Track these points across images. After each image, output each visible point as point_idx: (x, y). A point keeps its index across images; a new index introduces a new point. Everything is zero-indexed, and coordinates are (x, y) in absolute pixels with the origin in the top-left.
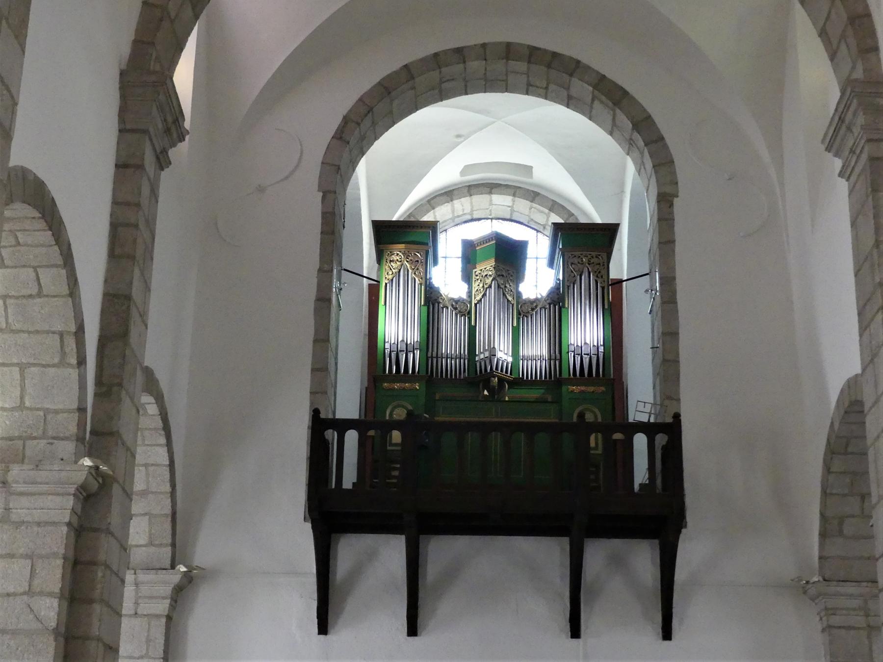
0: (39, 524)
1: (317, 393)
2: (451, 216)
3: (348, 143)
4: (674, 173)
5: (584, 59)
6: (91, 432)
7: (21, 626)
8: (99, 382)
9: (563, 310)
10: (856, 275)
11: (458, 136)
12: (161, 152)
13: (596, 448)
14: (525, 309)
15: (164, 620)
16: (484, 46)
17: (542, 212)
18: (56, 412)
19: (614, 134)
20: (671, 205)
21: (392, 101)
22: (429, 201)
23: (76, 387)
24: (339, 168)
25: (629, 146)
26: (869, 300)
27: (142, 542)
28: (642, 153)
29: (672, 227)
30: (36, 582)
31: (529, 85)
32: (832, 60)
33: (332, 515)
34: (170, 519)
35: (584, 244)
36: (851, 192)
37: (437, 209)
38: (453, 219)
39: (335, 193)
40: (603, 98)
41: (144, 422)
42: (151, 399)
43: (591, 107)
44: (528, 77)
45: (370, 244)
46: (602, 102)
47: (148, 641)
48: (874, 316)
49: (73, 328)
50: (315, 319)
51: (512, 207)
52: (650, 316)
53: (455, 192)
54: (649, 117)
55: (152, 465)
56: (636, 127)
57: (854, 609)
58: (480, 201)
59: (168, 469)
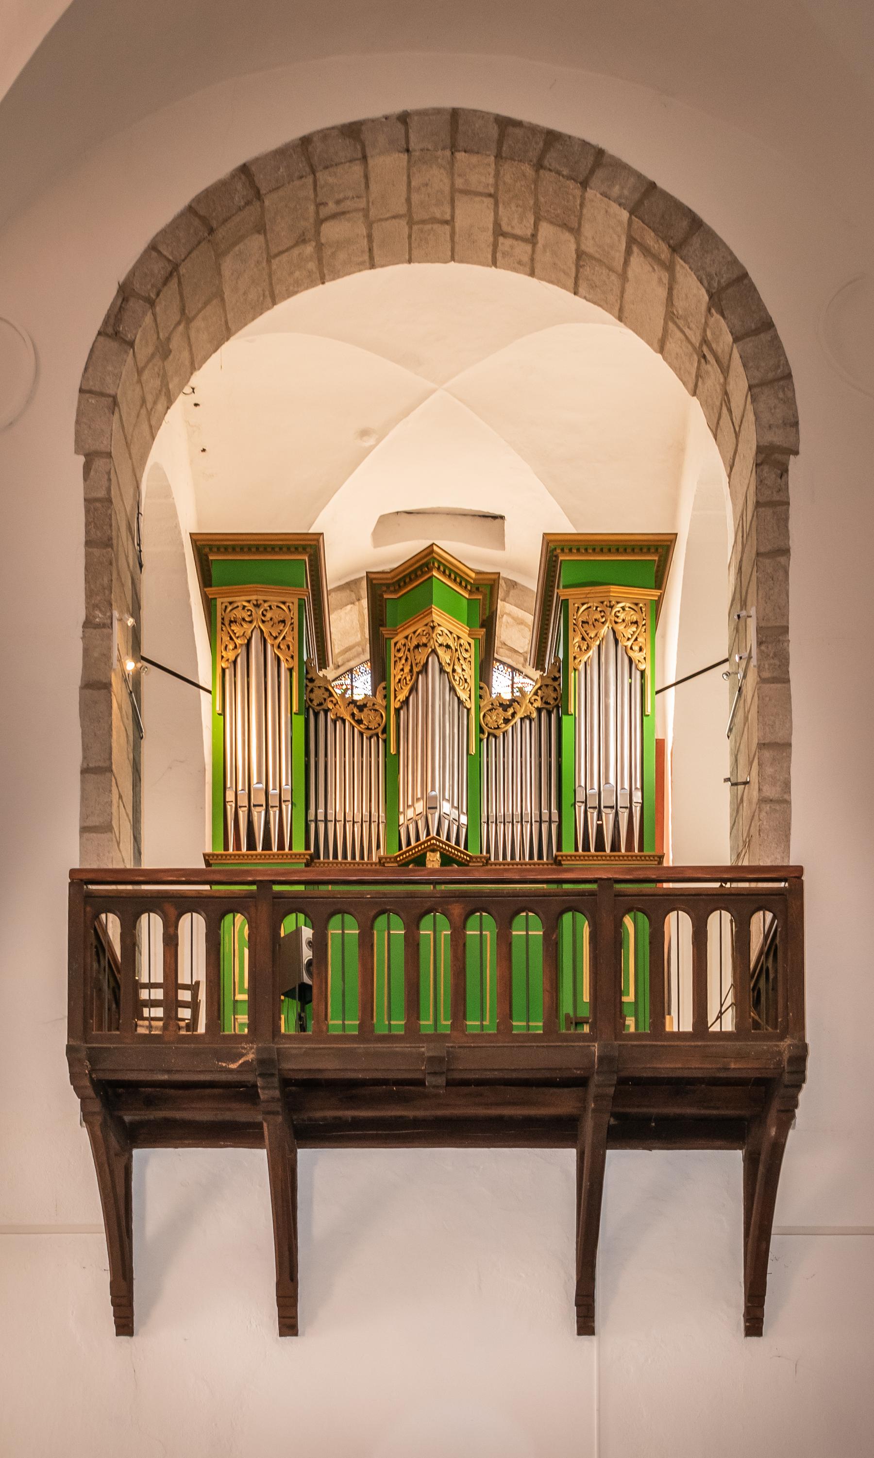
3: (131, 344)
4: (790, 402)
11: (364, 433)
16: (404, 118)
20: (783, 471)
21: (220, 255)
24: (115, 402)
28: (725, 371)
29: (783, 521)
31: (499, 232)
39: (109, 455)
43: (623, 277)
50: (82, 726)
52: (728, 741)
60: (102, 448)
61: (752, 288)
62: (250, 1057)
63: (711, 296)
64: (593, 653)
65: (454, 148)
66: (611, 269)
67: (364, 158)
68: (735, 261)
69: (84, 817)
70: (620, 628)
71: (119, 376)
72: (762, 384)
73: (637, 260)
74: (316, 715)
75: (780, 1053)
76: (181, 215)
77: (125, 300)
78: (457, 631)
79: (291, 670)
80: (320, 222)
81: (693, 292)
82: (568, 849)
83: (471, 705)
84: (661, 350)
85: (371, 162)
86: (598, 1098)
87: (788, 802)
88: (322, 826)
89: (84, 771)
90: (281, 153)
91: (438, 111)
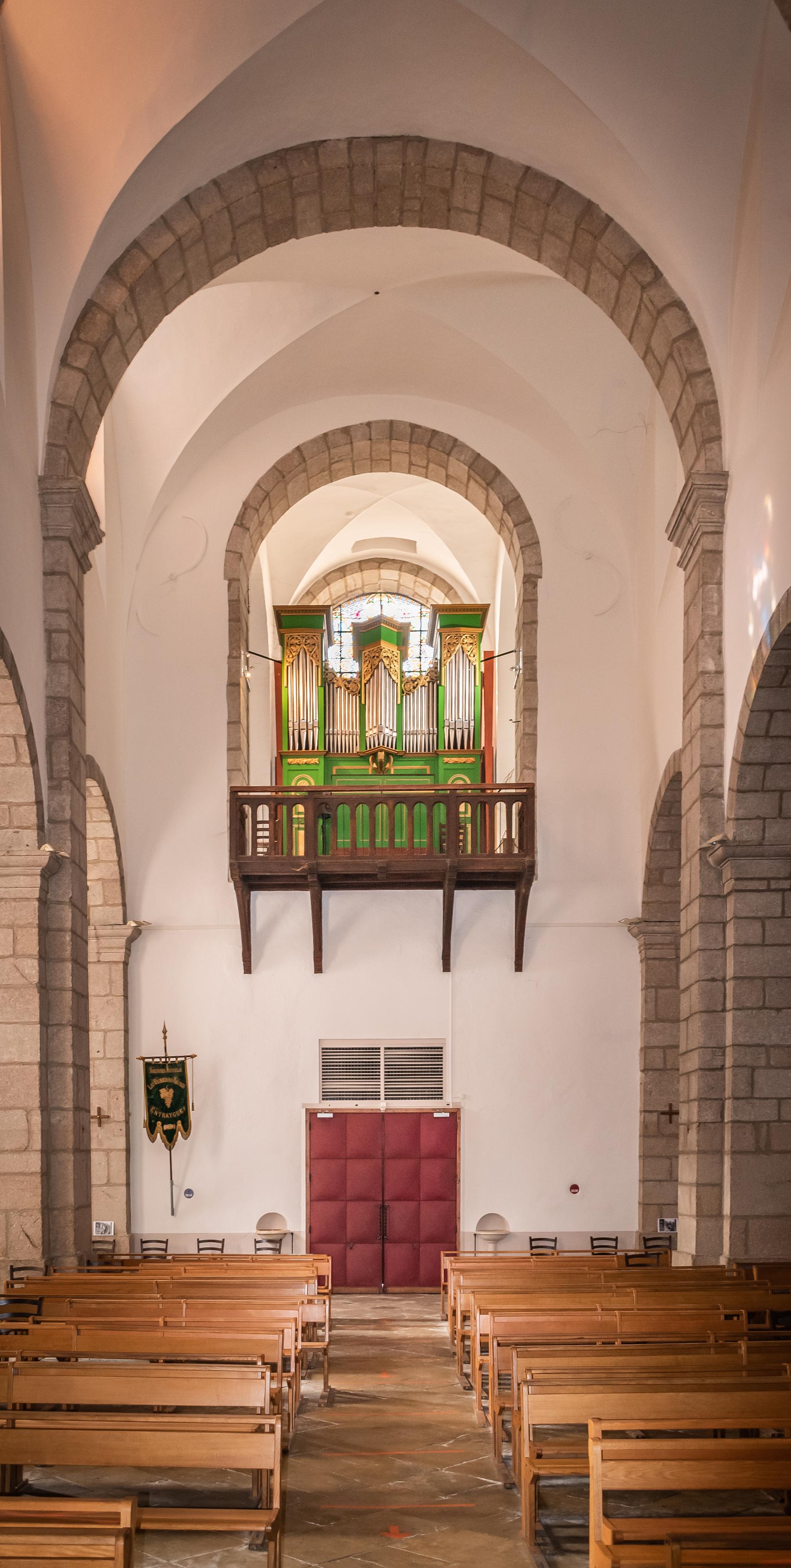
0: (15, 900)
1: (234, 770)
2: (344, 591)
3: (248, 529)
4: (539, 554)
5: (462, 438)
6: (49, 821)
7: (10, 982)
8: (51, 778)
9: (440, 688)
10: (684, 662)
11: (348, 513)
12: (83, 556)
13: (466, 812)
14: (410, 686)
15: (121, 966)
16: (369, 424)
17: (425, 586)
18: (19, 805)
19: (488, 513)
20: (535, 585)
21: (286, 484)
22: (324, 578)
23: (32, 783)
24: (241, 556)
25: (501, 526)
26: (693, 685)
27: (99, 903)
28: (511, 534)
29: (535, 608)
30: (18, 947)
31: (411, 464)
32: (680, 446)
33: (249, 879)
34: (119, 883)
35: (461, 620)
36: (687, 581)
37: (332, 585)
38: (346, 594)
39: (239, 580)
40: (478, 478)
41: (90, 802)
42: (94, 783)
43: (467, 486)
44: (410, 456)
45: (274, 633)
46: (476, 481)
47: (111, 982)
48: (696, 701)
49: (24, 732)
51: (398, 581)
53: (348, 568)
54: (519, 496)
55: (101, 838)
56: (506, 508)
57: (667, 944)
58: (370, 575)
59: (113, 841)
60: (235, 577)
61: (522, 502)
62: (305, 867)
63: (504, 506)
64: (453, 657)
65: (391, 438)
66: (461, 482)
67: (351, 443)
68: (515, 490)
69: (229, 744)
70: (465, 646)
71: (243, 544)
72: (526, 546)
73: (472, 482)
74: (329, 685)
75: (524, 863)
76: (270, 470)
77: (246, 509)
78: (392, 650)
79: (318, 666)
80: (331, 464)
81: (496, 502)
82: (441, 748)
83: (398, 681)
84: (485, 513)
85: (354, 444)
86: (449, 880)
87: (536, 735)
88: (331, 737)
89: (229, 723)
90: (314, 441)
91: (384, 421)
